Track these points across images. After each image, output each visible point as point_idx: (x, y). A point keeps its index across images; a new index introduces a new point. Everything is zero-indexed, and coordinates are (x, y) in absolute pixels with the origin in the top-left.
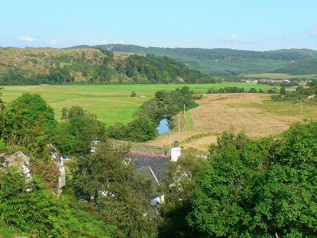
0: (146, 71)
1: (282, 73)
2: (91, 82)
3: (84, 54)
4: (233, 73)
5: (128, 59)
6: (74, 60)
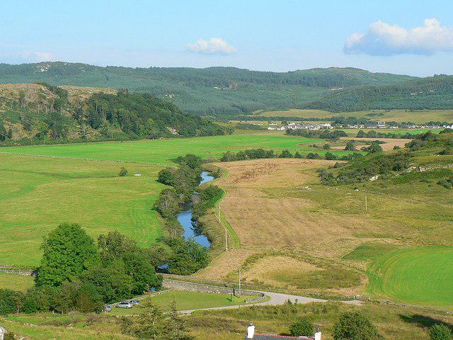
0: (121, 119)
1: (317, 108)
2: (39, 139)
3: (22, 95)
4: (244, 110)
5: (91, 101)
6: (8, 104)
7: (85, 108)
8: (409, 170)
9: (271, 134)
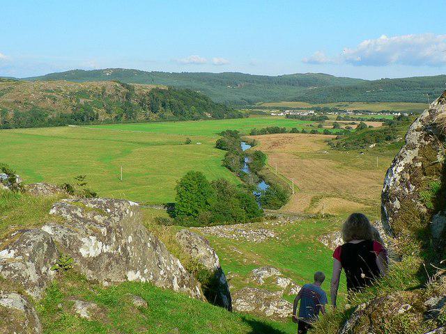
1: (304, 101)
2: (117, 120)
3: (104, 89)
4: (250, 102)
5: (150, 94)
6: (94, 96)
7: (147, 98)
8: (398, 140)
9: (273, 118)
